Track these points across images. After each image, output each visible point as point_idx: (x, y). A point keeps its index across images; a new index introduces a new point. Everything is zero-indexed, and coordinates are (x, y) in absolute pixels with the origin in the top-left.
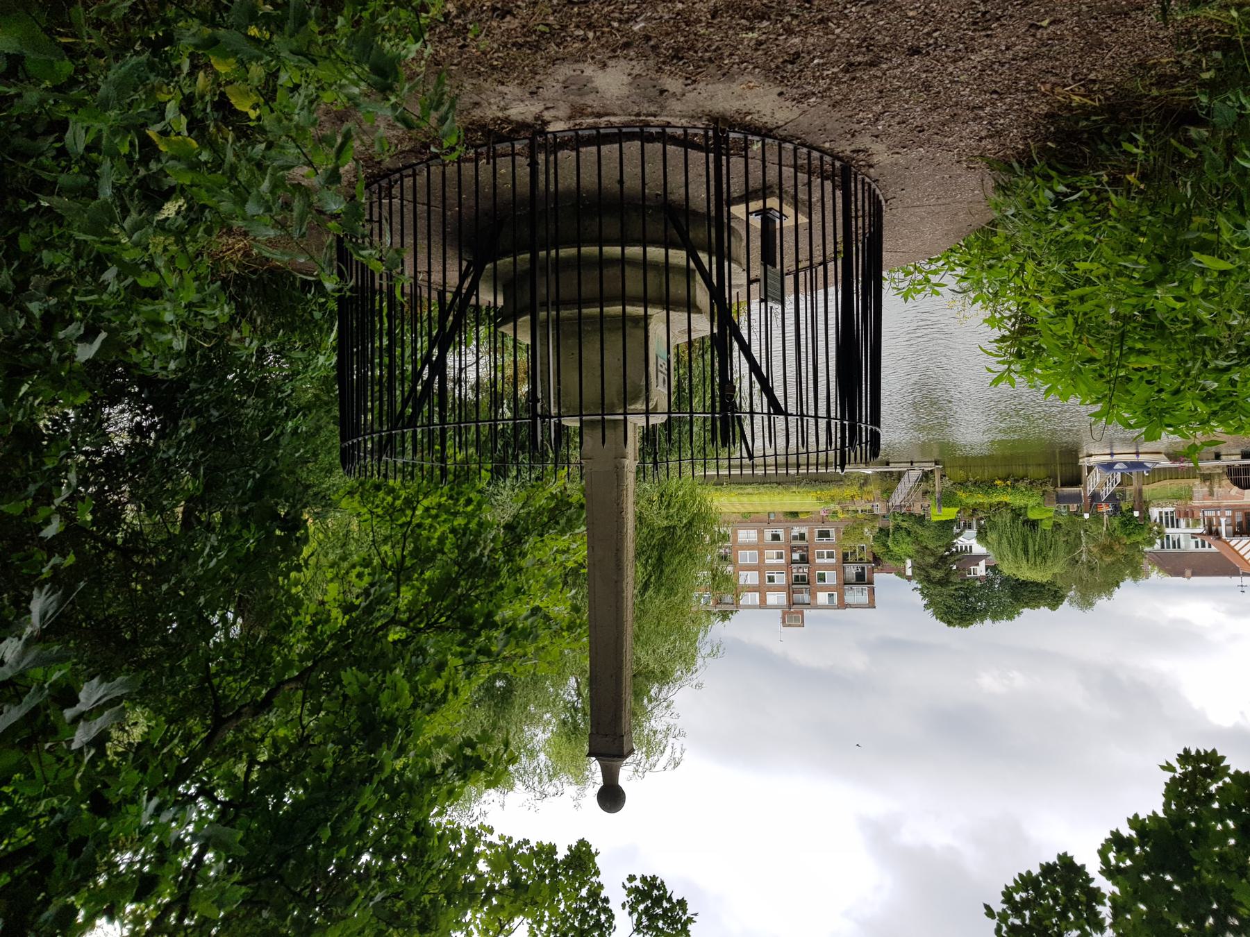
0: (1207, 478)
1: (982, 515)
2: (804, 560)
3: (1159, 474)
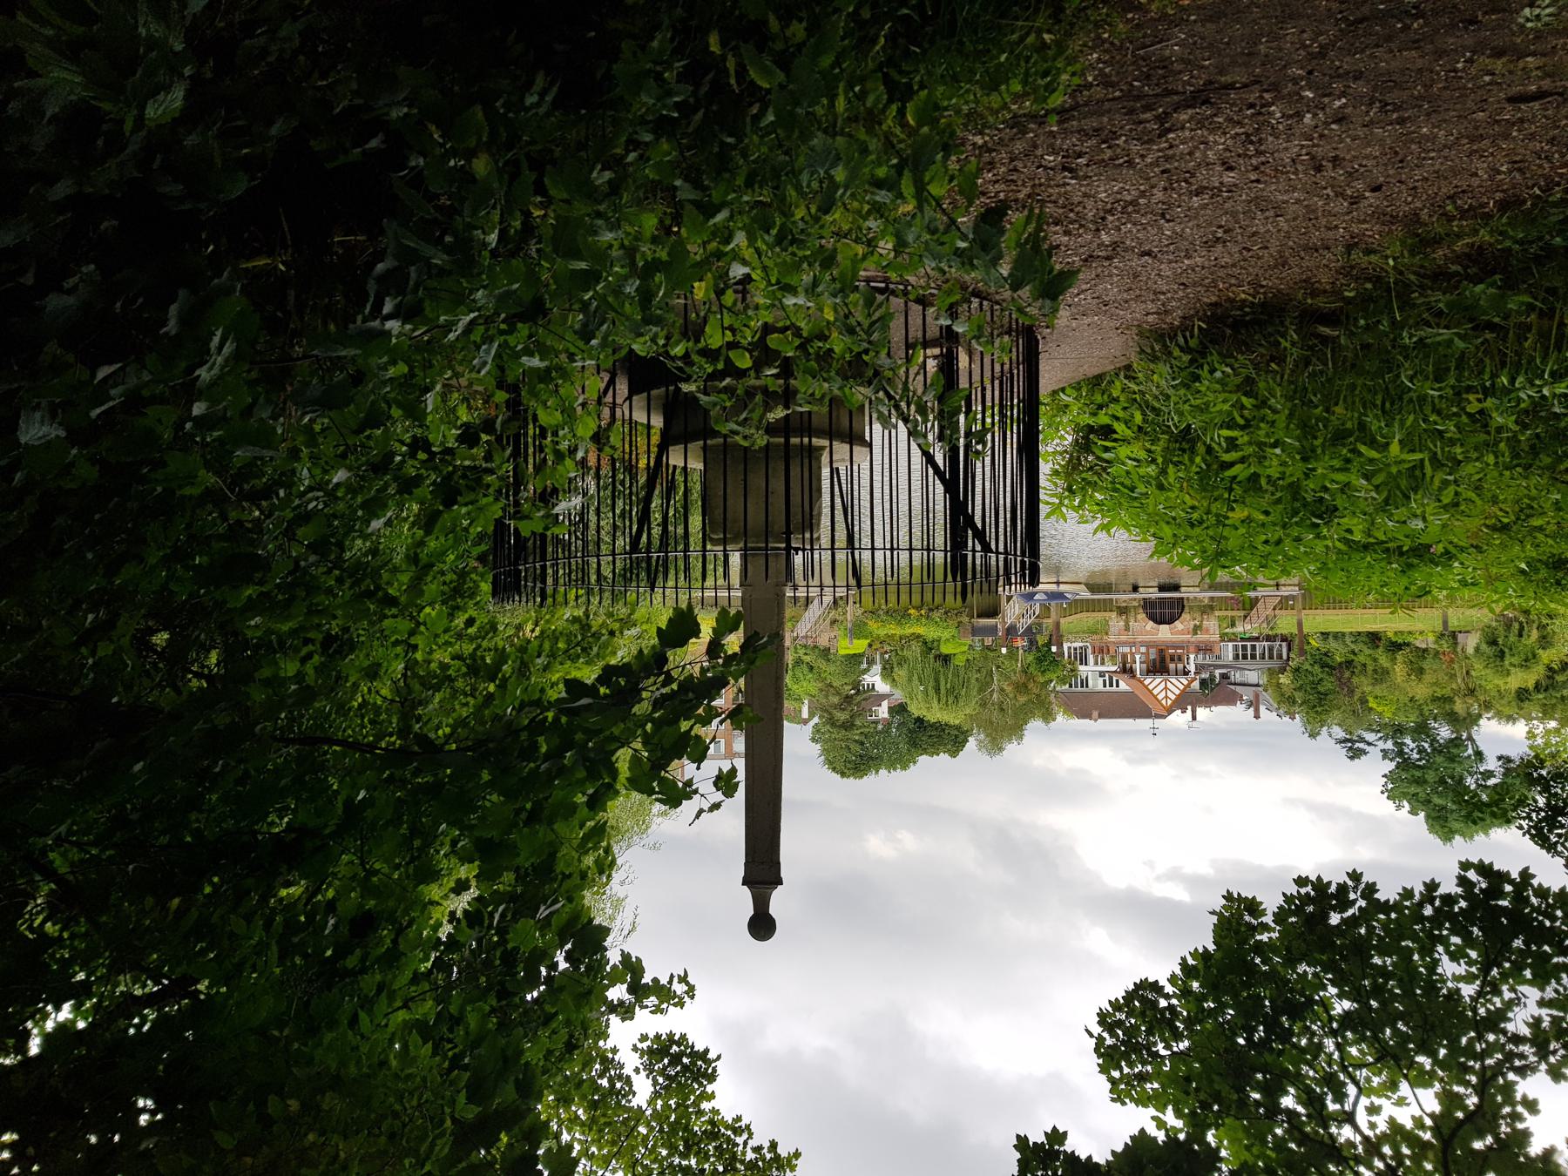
0: (1123, 611)
1: (888, 648)
3: (1080, 606)
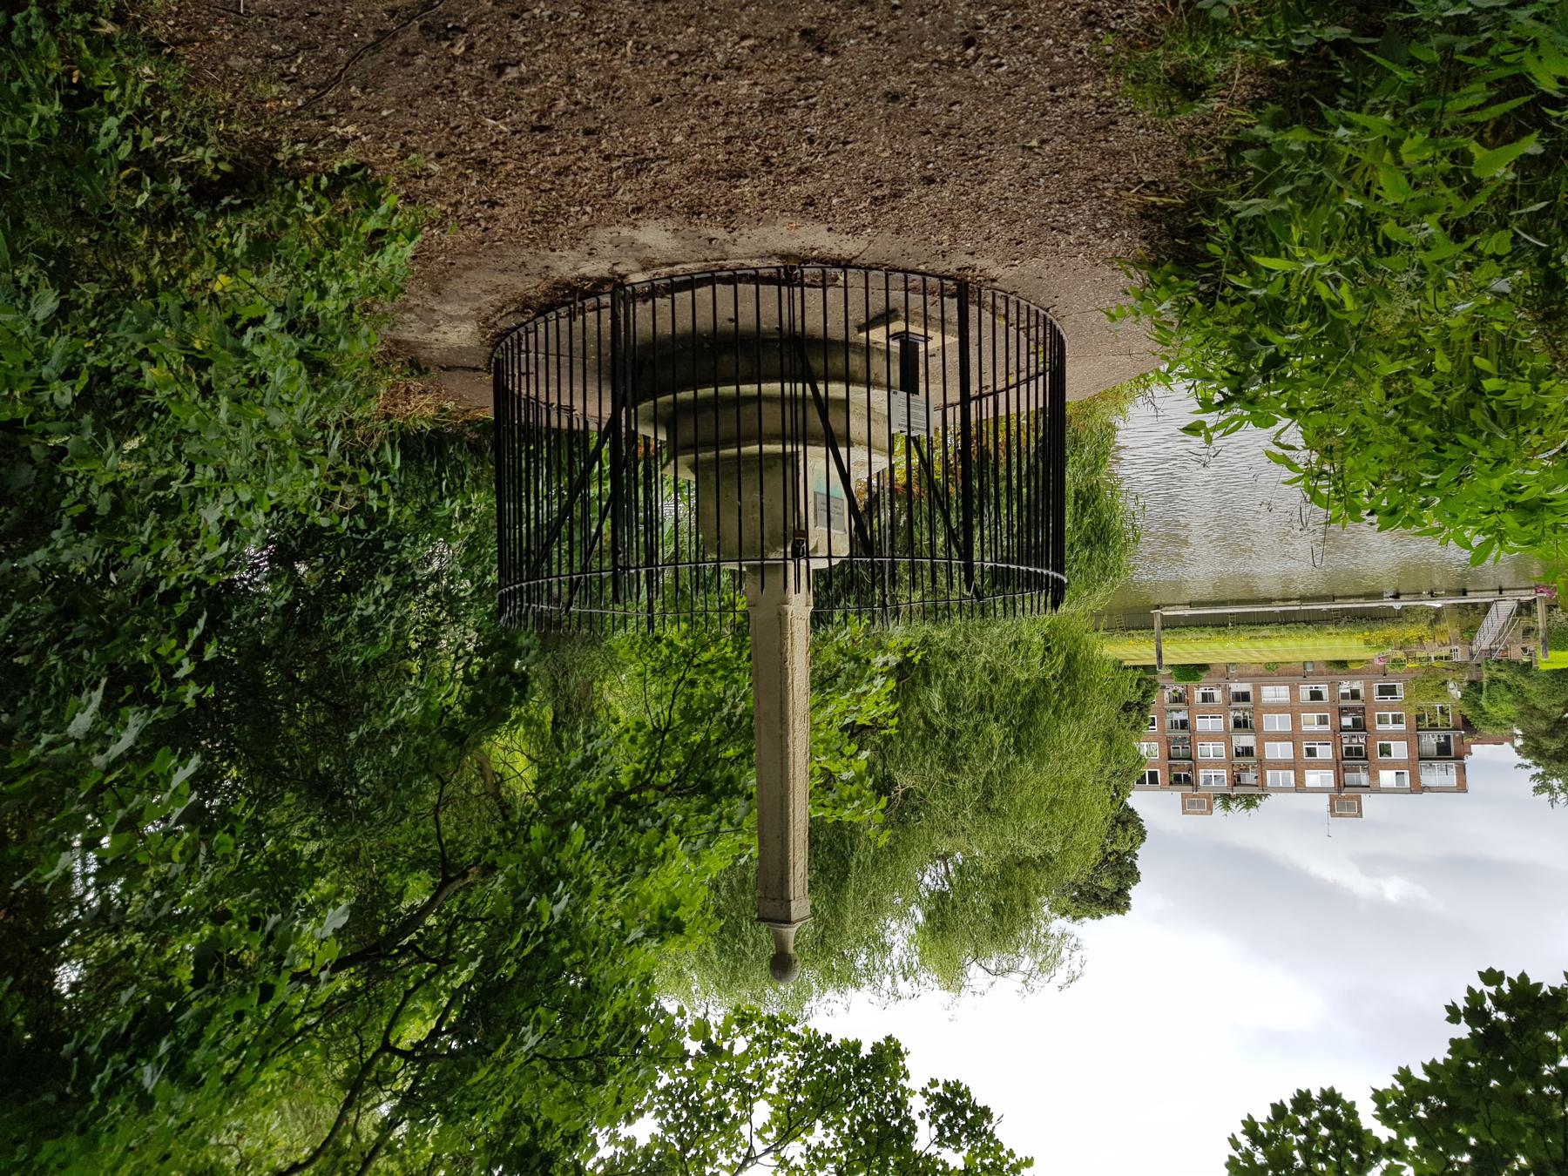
2: (1358, 726)
